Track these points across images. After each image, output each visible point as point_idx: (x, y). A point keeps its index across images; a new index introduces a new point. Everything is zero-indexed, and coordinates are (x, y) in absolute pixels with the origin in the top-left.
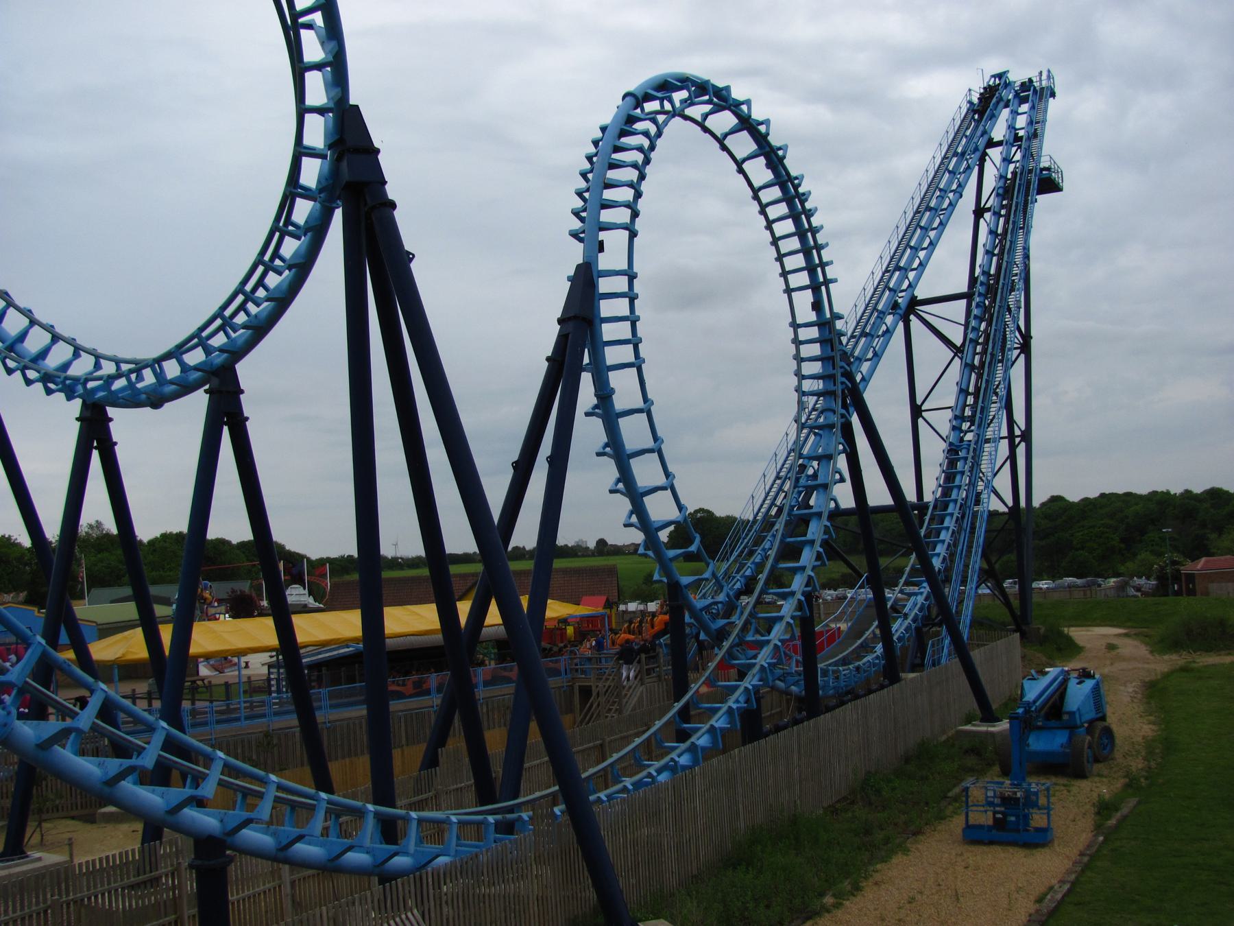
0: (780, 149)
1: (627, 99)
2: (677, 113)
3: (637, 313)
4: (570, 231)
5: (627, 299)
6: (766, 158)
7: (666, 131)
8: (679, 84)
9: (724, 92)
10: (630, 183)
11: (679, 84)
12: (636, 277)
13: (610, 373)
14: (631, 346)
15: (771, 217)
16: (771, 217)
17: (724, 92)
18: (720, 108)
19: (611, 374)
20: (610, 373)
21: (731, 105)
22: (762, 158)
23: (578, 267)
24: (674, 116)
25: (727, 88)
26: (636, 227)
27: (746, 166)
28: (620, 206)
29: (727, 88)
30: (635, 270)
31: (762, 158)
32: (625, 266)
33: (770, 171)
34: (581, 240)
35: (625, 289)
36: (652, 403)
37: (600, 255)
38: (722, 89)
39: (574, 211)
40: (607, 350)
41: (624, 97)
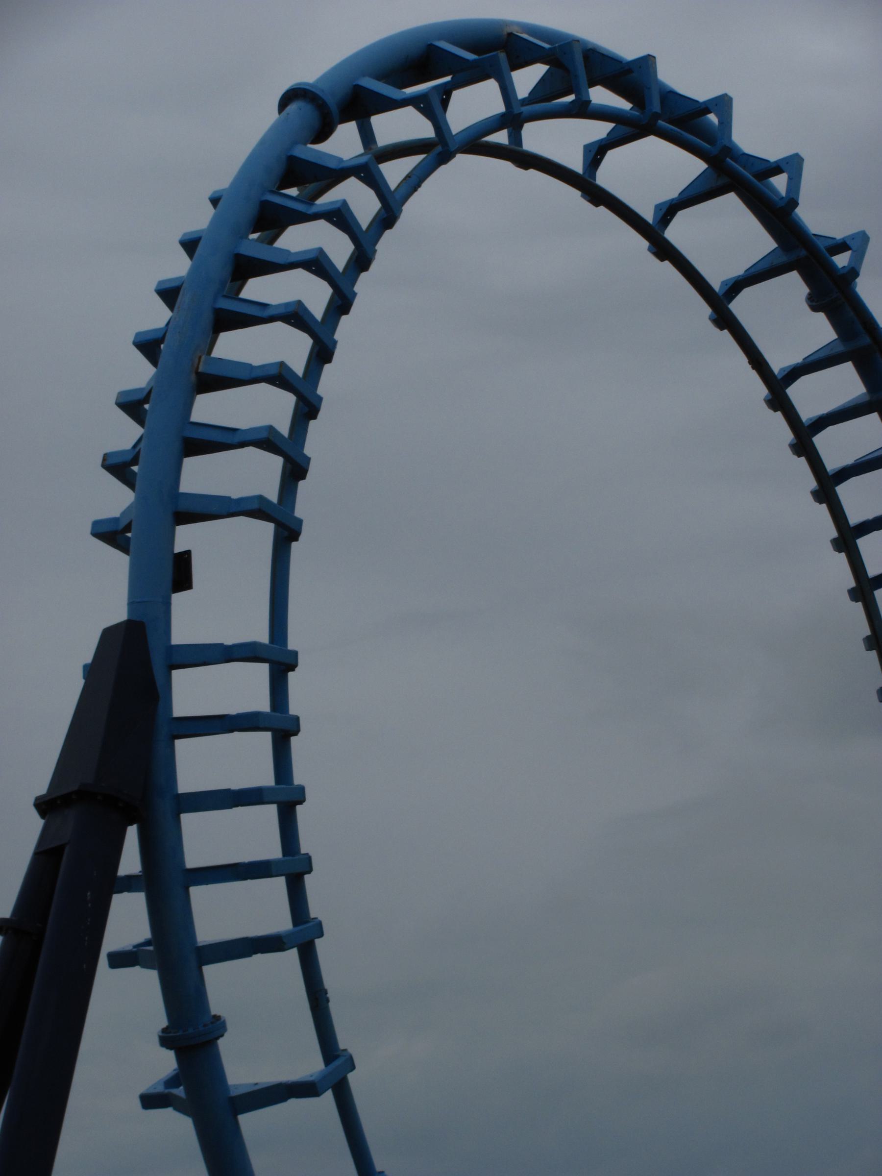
0: (841, 247)
1: (293, 107)
2: (332, 102)
3: (298, 778)
4: (96, 524)
5: (268, 735)
6: (808, 278)
7: (411, 210)
8: (470, 56)
9: (713, 118)
10: (274, 371)
11: (470, 56)
12: (292, 667)
13: (209, 971)
14: (280, 883)
15: (832, 464)
16: (832, 464)
17: (713, 118)
18: (625, 130)
19: (213, 973)
20: (209, 971)
21: (656, 116)
22: (794, 277)
23: (108, 634)
24: (445, 157)
25: (647, 63)
26: (299, 513)
27: (739, 307)
28: (242, 445)
29: (647, 63)
30: (292, 644)
31: (794, 277)
32: (261, 634)
33: (821, 317)
34: (123, 546)
35: (262, 703)
36: (351, 1065)
37: (178, 599)
38: (705, 108)
39: (111, 461)
40: (199, 894)
41: (285, 101)
